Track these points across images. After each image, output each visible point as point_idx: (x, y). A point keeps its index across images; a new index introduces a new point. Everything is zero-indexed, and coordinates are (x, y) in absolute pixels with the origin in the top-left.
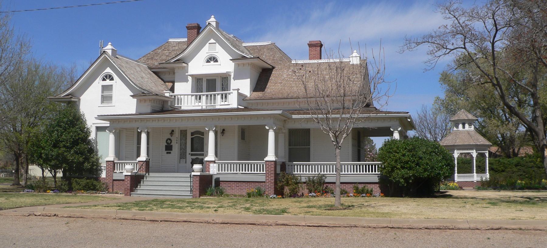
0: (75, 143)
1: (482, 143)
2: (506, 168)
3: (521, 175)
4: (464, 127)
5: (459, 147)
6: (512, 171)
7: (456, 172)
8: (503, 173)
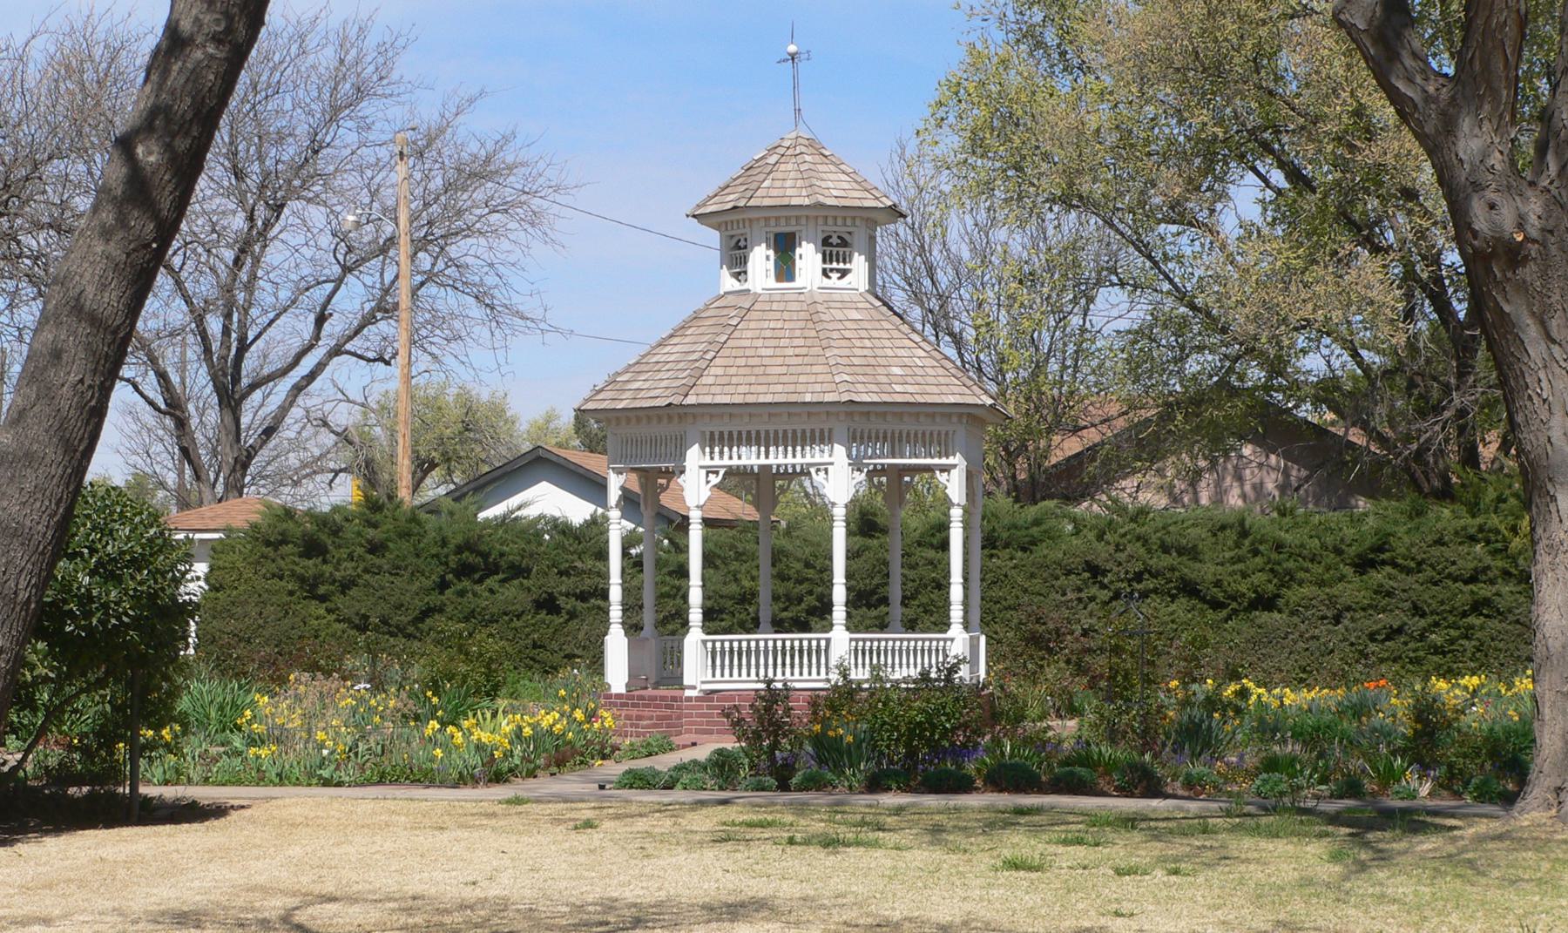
1: (901, 393)
2: (1287, 579)
3: (1394, 633)
4: (785, 270)
6: (1332, 601)
7: (695, 616)
8: (1264, 617)
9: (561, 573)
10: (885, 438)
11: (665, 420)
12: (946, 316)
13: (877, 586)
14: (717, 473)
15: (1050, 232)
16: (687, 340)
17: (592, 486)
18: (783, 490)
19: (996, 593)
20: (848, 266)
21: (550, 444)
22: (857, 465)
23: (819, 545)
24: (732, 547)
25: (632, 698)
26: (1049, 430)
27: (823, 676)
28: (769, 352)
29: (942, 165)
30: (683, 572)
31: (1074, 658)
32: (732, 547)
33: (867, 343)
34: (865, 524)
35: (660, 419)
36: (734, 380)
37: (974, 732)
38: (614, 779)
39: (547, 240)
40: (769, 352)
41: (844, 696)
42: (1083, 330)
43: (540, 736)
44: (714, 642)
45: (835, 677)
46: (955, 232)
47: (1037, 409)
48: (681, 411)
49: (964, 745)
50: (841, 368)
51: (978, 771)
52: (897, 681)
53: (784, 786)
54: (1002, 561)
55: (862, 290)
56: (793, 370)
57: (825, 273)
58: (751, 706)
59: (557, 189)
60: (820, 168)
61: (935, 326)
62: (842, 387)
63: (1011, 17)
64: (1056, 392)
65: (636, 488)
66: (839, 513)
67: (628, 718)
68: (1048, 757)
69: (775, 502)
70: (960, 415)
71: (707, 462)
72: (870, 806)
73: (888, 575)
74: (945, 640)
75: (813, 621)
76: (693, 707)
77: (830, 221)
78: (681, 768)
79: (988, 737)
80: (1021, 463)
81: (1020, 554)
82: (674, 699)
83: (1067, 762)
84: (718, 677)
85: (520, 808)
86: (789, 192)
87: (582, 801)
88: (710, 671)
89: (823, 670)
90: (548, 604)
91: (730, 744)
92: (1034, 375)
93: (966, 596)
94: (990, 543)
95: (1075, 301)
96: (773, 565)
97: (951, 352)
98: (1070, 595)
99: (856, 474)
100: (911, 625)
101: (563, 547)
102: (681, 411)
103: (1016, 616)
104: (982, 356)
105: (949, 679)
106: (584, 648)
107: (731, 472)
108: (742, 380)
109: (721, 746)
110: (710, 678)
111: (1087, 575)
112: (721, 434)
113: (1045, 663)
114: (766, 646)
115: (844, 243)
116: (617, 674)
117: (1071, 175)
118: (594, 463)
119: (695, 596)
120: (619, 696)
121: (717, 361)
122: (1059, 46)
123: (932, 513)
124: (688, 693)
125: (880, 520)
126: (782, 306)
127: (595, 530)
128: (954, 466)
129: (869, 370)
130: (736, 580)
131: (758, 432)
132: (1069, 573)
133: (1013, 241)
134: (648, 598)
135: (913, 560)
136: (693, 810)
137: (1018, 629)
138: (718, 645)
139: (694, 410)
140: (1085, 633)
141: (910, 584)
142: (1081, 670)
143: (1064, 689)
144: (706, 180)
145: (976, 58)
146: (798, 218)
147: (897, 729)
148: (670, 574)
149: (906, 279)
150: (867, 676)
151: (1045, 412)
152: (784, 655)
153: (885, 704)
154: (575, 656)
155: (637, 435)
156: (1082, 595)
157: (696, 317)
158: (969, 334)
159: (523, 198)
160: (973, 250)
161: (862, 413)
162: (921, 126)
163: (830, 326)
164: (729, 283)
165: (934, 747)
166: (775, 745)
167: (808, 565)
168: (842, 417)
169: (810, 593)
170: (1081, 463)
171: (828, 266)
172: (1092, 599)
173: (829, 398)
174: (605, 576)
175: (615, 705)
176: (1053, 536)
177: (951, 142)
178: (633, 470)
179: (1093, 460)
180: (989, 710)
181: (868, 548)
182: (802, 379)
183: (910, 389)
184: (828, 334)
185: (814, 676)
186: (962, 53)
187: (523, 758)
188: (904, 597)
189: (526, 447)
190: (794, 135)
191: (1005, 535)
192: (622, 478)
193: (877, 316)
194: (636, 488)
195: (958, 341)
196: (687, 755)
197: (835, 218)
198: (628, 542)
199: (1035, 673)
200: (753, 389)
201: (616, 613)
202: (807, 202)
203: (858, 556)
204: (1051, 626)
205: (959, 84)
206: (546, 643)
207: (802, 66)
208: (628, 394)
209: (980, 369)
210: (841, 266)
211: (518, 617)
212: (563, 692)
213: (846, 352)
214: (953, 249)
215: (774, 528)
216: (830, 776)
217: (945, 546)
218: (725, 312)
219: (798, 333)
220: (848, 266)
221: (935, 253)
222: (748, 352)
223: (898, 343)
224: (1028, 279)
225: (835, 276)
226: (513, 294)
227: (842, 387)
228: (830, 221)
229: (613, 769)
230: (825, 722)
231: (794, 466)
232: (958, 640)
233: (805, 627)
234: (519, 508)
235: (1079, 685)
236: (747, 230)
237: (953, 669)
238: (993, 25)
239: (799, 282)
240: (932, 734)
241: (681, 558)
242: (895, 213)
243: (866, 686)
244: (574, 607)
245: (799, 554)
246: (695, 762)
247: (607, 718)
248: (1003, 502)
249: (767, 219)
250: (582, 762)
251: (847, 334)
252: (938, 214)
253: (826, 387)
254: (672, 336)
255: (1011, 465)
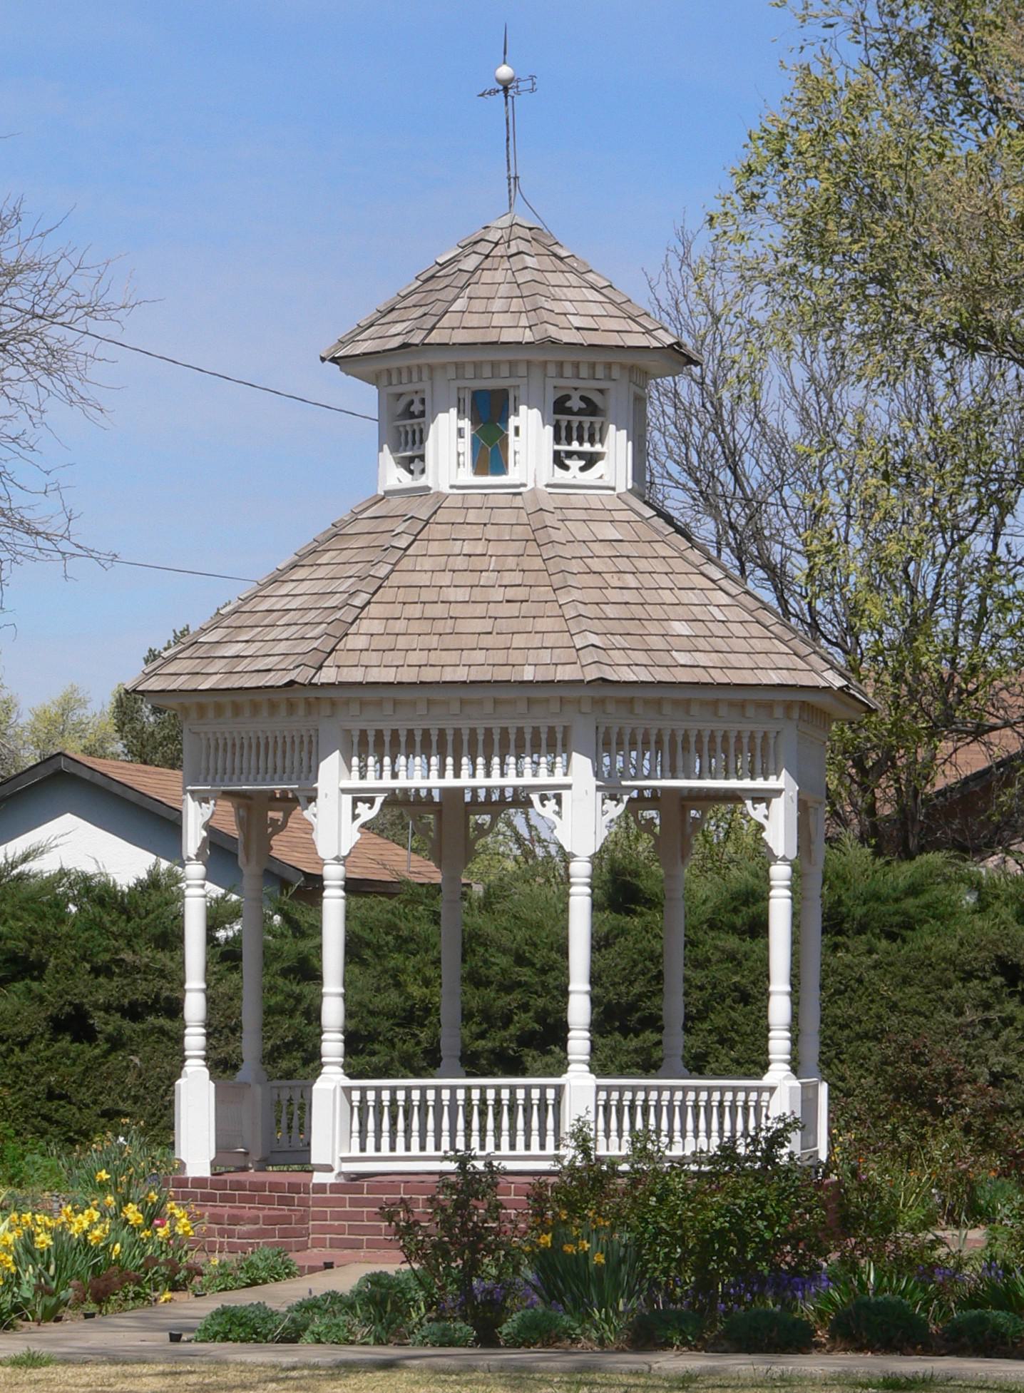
0: (727, 770)
1: (688, 665)
4: (490, 452)
5: (387, 718)
7: (332, 1046)
9: (96, 971)
10: (659, 743)
11: (229, 712)
12: (757, 535)
13: (640, 996)
14: (371, 801)
15: (940, 390)
16: (321, 572)
17: (157, 826)
18: (482, 831)
19: (843, 1009)
20: (598, 448)
21: (74, 748)
22: (610, 791)
23: (540, 926)
24: (391, 928)
25: (223, 1185)
26: (933, 733)
27: (550, 1150)
28: (462, 594)
29: (750, 274)
30: (310, 972)
31: (977, 1123)
32: (391, 928)
33: (631, 581)
34: (620, 890)
35: (273, 706)
36: (402, 642)
37: (809, 1248)
38: (197, 1324)
39: (75, 399)
40: (462, 594)
41: (588, 1183)
42: (993, 561)
43: (69, 1251)
44: (363, 1090)
45: (568, 1152)
46: (775, 390)
47: (913, 694)
48: (312, 694)
49: (795, 1271)
50: (586, 624)
51: (820, 1314)
52: (682, 1160)
53: (487, 1339)
54: (855, 955)
55: (621, 489)
56: (502, 625)
57: (559, 460)
58: (431, 1201)
59: (90, 310)
60: (553, 278)
61: (740, 553)
62: (588, 656)
63: (874, 19)
64: (945, 668)
65: (230, 827)
66: (580, 870)
67: (216, 1219)
68: (939, 1292)
69: (469, 854)
70: (788, 706)
71: (355, 782)
72: (637, 1373)
73: (659, 977)
74: (760, 1090)
75: (529, 1056)
76: (326, 1202)
77: (568, 371)
78: (311, 1306)
79: (834, 1256)
80: (885, 789)
81: (884, 944)
82: (294, 1188)
83: (973, 1301)
84: (371, 1151)
85: (36, 1373)
86: (498, 320)
87: (144, 1362)
88: (356, 1141)
89: (550, 1140)
90: (74, 1024)
91: (393, 1265)
92: (909, 637)
93: (795, 1017)
94: (834, 923)
95: (979, 510)
96: (464, 961)
97: (769, 597)
98: (970, 1015)
99: (610, 804)
100: (697, 1065)
101: (101, 926)
102: (312, 694)
103: (876, 1052)
104: (819, 605)
105: (769, 1157)
106: (136, 1099)
107: (396, 800)
108: (415, 642)
109: (377, 1268)
110: (356, 1152)
111: (999, 980)
112: (379, 734)
113: (928, 1130)
114: (453, 1098)
115: (591, 408)
116: (196, 1141)
117: (976, 293)
118: (155, 782)
119: (333, 1011)
120: (199, 1182)
121: (373, 610)
122: (956, 70)
123: (734, 872)
124: (318, 1178)
125: (645, 884)
126: (484, 516)
127: (156, 897)
128: (778, 792)
129: (632, 627)
130: (398, 985)
131: (442, 733)
132: (968, 976)
133: (874, 407)
134: (250, 1015)
135: (699, 953)
136: (333, 1377)
137: (881, 1073)
138: (371, 1095)
139: (333, 694)
140: (996, 1080)
141: (696, 994)
142: (987, 1142)
143: (961, 1177)
144: (358, 294)
145: (815, 93)
146: (512, 364)
147: (682, 1241)
148: (285, 973)
149: (690, 471)
150: (625, 1151)
151: (926, 699)
152: (483, 1114)
153: (660, 1200)
154: (120, 1114)
155: (224, 734)
156: (992, 1015)
157: (336, 533)
158: (798, 567)
159: (34, 325)
160: (805, 419)
161: (619, 701)
162: (716, 208)
163: (567, 551)
164: (393, 476)
165: (744, 1271)
166: (473, 1267)
167: (521, 960)
168: (586, 708)
169: (525, 1007)
170: (987, 789)
171: (563, 448)
172: (1008, 1021)
173: (564, 674)
174: (177, 977)
175: (193, 1196)
176: (943, 915)
177: (768, 236)
178: (227, 795)
179: (1009, 783)
180: (845, 1210)
181: (623, 932)
182: (519, 641)
183: (702, 659)
184: (564, 565)
185: (535, 1150)
186: (787, 84)
187: (38, 1288)
188: (688, 1017)
189: (30, 757)
190: (506, 221)
191: (859, 911)
192: (208, 809)
193: (647, 534)
194: (230, 827)
195: (777, 576)
196: (320, 1284)
197: (560, 365)
198: (215, 918)
199: (909, 1148)
200: (434, 657)
201: (195, 1039)
202: (528, 336)
203: (608, 945)
204: (939, 1068)
205: (783, 135)
206: (70, 1089)
207: (521, 101)
208: (218, 665)
209: (814, 626)
210: (587, 447)
211: (23, 1045)
212: (103, 1175)
213: (595, 595)
214: (772, 419)
215: (464, 896)
216: (566, 1320)
217: (759, 928)
218: (385, 525)
219: (511, 563)
220: (598, 448)
221: (741, 425)
222: (427, 595)
223: (683, 581)
224: (899, 472)
225: (575, 464)
226: (14, 491)
227: (588, 656)
228: (568, 371)
229: (194, 1308)
230: (557, 1228)
231: (502, 789)
232: (781, 1089)
233: (515, 1067)
234: (25, 858)
235: (987, 1169)
236: (425, 385)
237: (777, 1139)
238: (843, 33)
239: (514, 475)
240: (742, 1251)
241: (305, 945)
242: (678, 357)
243: (625, 1167)
244: (119, 1030)
245: (506, 941)
246: (333, 1296)
247: (181, 1220)
248: (858, 855)
249: (459, 366)
250: (137, 1296)
251: (596, 565)
252: (745, 361)
253: (560, 655)
254: (294, 566)
255: (865, 788)
